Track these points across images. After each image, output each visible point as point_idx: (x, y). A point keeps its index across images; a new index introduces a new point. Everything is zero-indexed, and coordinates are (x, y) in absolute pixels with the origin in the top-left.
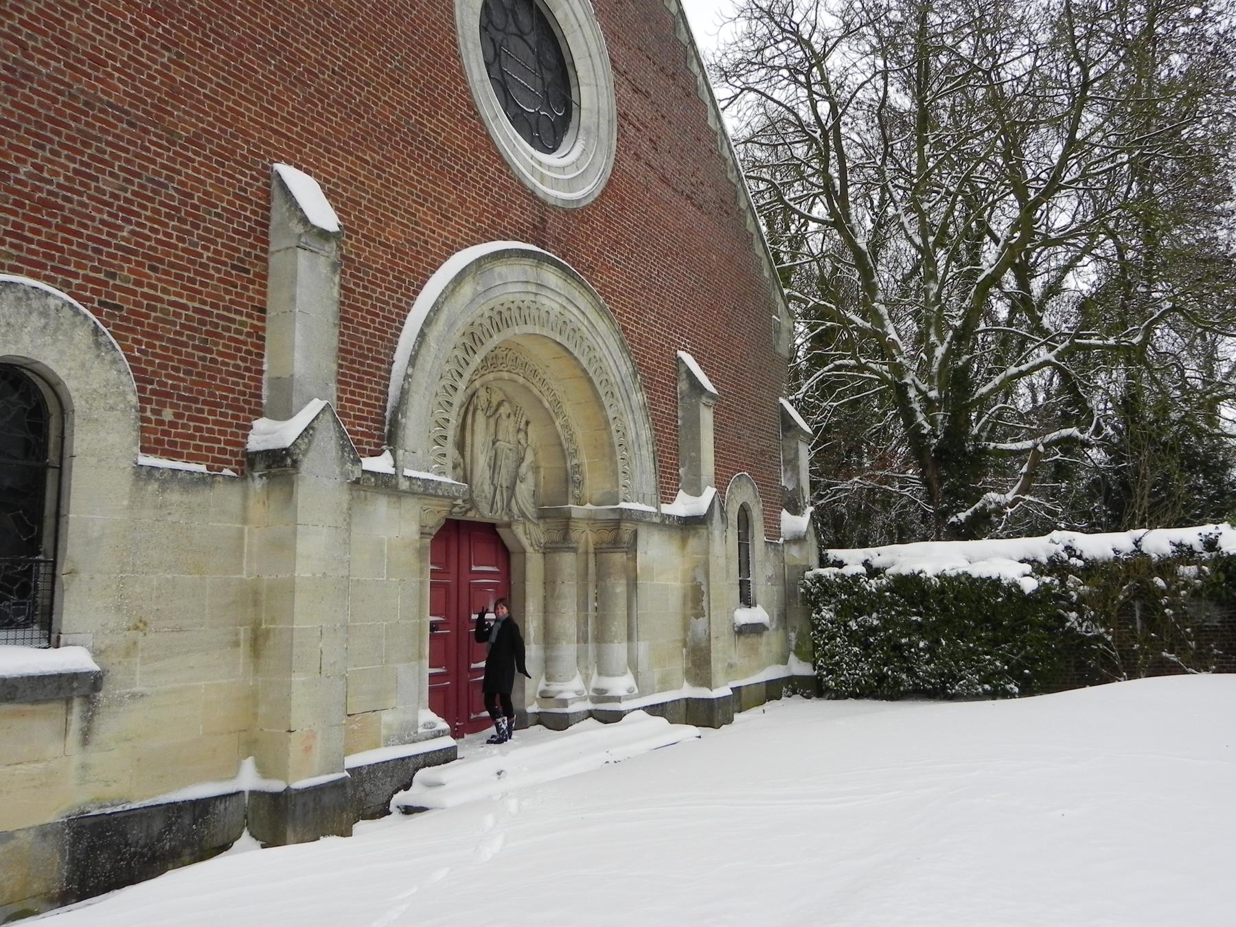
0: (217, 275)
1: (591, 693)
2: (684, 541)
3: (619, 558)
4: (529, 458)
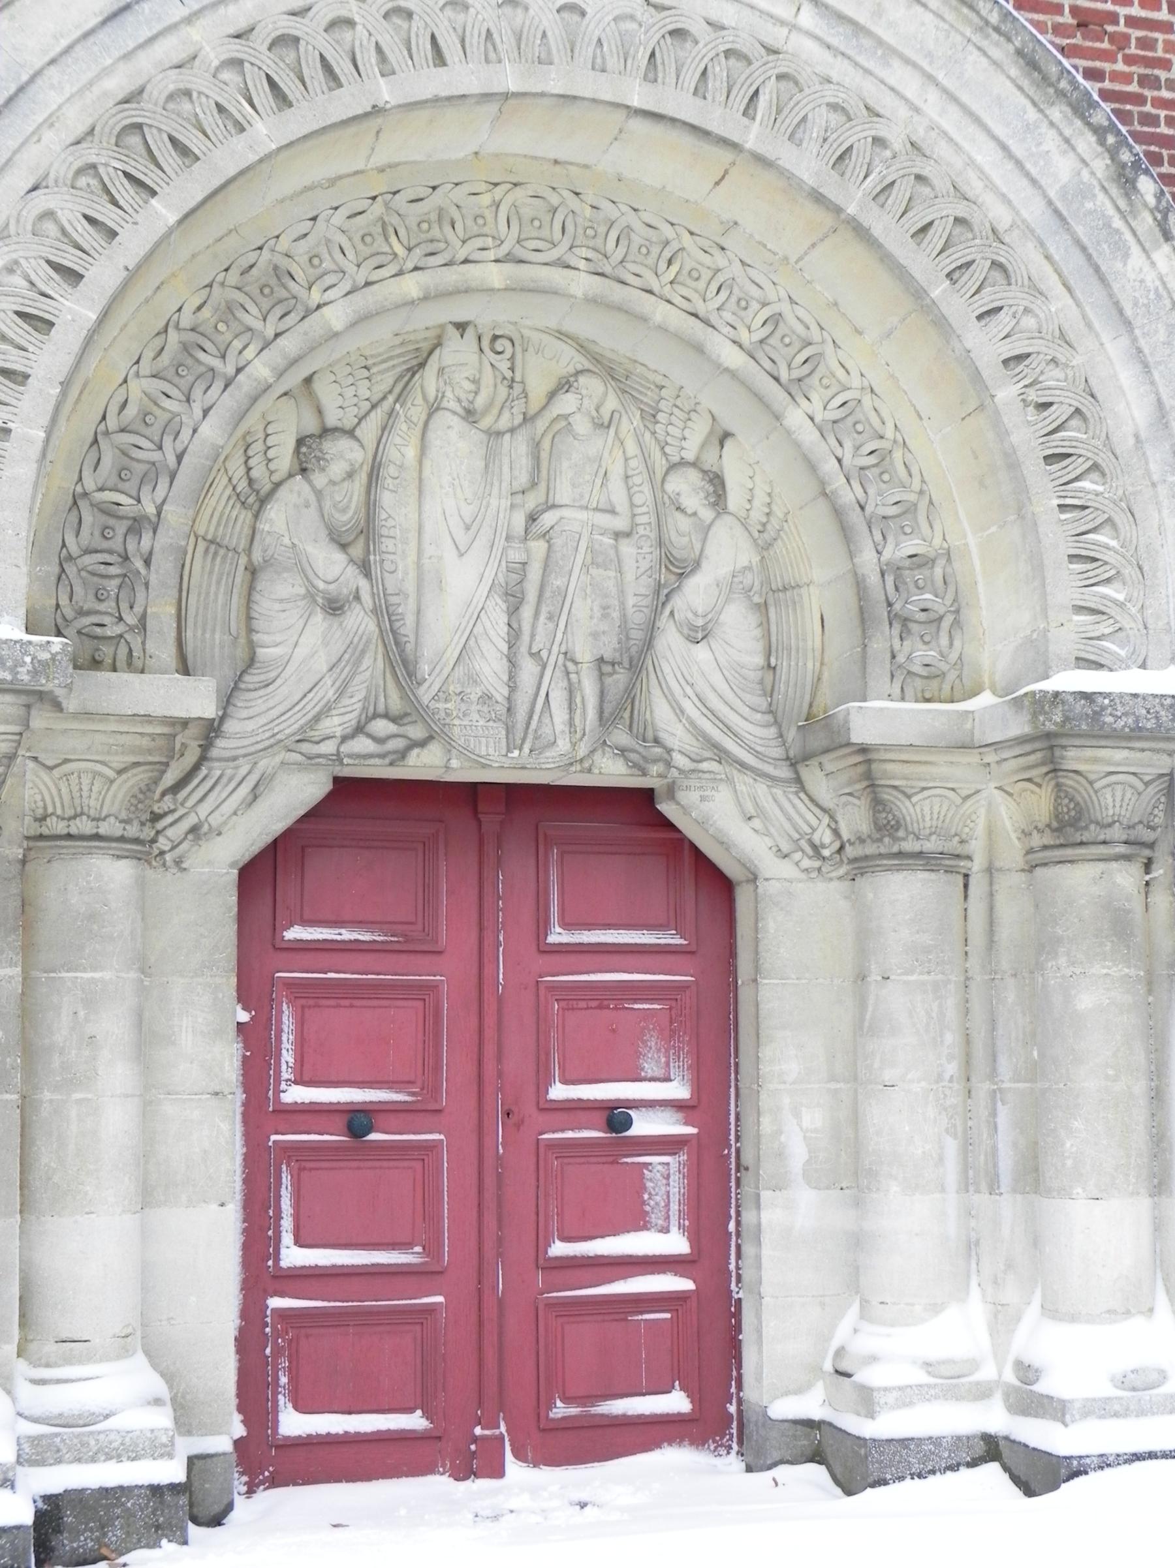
1: (1010, 1377)
4: (726, 553)
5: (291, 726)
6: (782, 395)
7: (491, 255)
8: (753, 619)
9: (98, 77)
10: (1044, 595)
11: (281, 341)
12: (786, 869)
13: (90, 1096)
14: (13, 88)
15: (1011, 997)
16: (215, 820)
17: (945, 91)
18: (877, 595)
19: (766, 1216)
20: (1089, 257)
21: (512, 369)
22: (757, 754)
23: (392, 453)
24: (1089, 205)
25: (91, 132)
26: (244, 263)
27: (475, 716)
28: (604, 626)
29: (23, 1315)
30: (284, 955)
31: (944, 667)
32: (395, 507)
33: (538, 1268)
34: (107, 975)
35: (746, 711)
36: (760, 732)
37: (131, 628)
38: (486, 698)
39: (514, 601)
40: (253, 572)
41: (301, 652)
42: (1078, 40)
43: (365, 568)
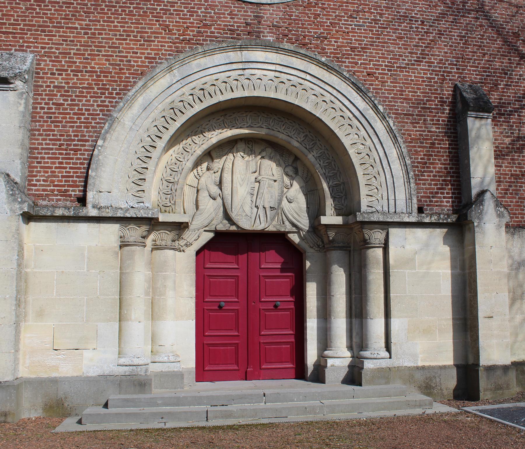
6: (307, 151)
7: (245, 126)
11: (203, 146)
12: (312, 250)
21: (220, 185)
27: (244, 219)
28: (271, 200)
31: (343, 207)
34: (168, 273)
42: (368, 78)
43: (221, 189)
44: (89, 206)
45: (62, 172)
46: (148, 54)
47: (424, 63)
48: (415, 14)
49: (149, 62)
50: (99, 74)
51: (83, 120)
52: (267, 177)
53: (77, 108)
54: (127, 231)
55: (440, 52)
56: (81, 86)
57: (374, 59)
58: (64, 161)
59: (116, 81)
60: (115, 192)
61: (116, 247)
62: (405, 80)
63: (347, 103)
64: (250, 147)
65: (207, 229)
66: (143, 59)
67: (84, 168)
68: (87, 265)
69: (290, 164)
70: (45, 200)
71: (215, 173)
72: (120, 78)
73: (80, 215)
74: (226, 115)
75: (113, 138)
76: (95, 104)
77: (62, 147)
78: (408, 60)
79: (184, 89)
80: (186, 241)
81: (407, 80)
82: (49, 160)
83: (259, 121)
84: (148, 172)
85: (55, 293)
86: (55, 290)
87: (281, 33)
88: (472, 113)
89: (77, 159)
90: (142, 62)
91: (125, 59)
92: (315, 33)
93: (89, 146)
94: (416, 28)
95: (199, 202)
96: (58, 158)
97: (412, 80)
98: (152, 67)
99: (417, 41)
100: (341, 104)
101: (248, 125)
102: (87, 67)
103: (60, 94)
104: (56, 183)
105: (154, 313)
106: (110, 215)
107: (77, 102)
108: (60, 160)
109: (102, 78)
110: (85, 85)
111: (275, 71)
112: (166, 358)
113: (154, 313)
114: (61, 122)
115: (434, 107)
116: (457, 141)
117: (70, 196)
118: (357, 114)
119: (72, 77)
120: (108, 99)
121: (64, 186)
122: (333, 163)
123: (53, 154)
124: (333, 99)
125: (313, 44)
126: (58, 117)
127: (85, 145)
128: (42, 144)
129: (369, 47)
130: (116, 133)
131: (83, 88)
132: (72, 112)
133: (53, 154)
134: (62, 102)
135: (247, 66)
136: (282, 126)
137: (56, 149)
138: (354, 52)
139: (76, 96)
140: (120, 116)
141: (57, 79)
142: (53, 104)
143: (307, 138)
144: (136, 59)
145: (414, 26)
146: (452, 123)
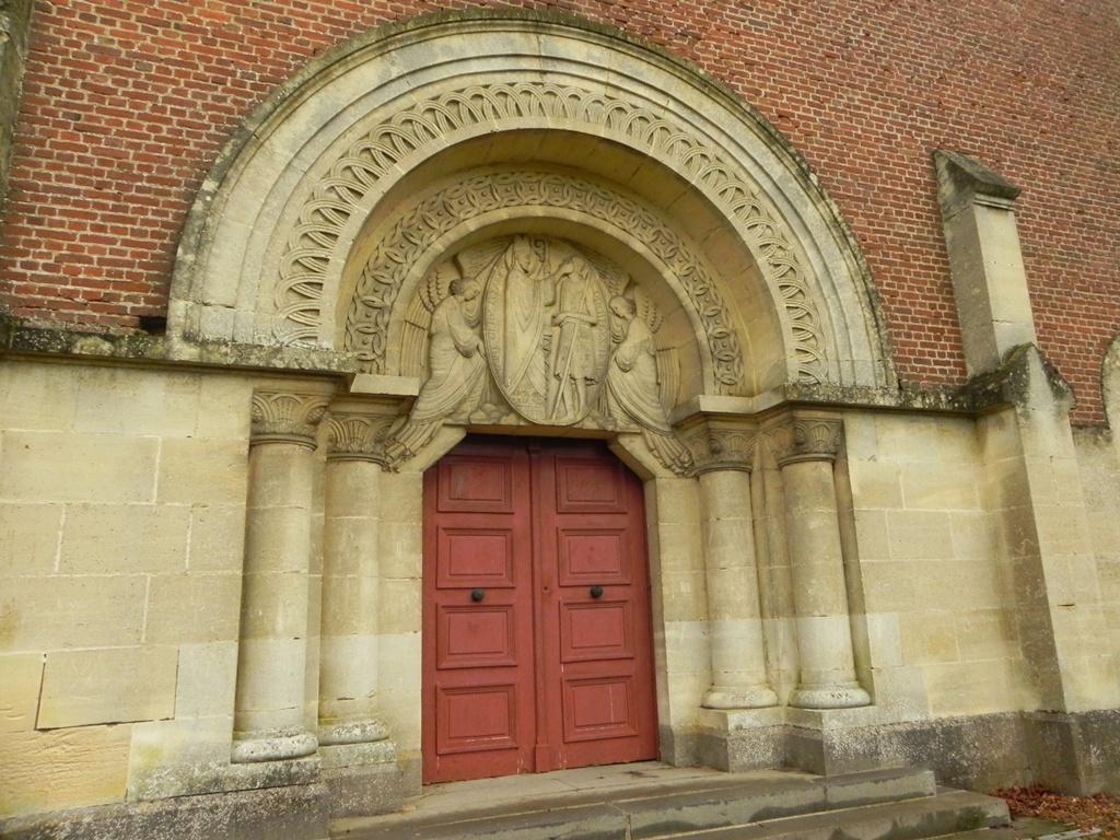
0: (1054, 301)
2: (979, 442)
3: (815, 473)
5: (448, 407)
7: (538, 202)
8: (651, 361)
9: (371, 112)
10: (783, 345)
12: (668, 473)
13: (356, 576)
14: (334, 114)
15: (775, 526)
16: (413, 448)
17: (729, 137)
18: (707, 348)
19: (668, 634)
20: (792, 206)
22: (655, 421)
23: (492, 287)
24: (790, 185)
25: (368, 135)
26: (431, 200)
29: (321, 687)
30: (443, 515)
32: (494, 311)
33: (437, 754)
34: (365, 518)
35: (649, 401)
36: (656, 411)
37: (379, 356)
38: (536, 393)
39: (547, 351)
40: (430, 337)
41: (453, 373)
43: (482, 337)
44: (175, 335)
45: (102, 251)
46: (331, 12)
47: (875, 108)
48: (853, 17)
49: (332, 30)
50: (210, 36)
51: (164, 134)
52: (576, 316)
53: (150, 104)
54: (273, 406)
55: (902, 91)
56: (163, 57)
57: (789, 89)
58: (109, 224)
59: (254, 59)
60: (246, 308)
61: (243, 442)
62: (847, 133)
63: (747, 163)
64: (541, 252)
65: (449, 421)
66: (319, 20)
67: (163, 246)
68: (159, 488)
69: (620, 292)
70: (46, 316)
71: (466, 300)
72: (264, 54)
73: (147, 354)
74: (496, 175)
75: (245, 181)
76: (199, 102)
77: (106, 191)
78: (848, 99)
79: (414, 98)
80: (403, 448)
81: (850, 134)
82: (65, 219)
83: (565, 195)
84: (329, 267)
85: (57, 563)
86: (58, 557)
87: (615, 16)
88: (982, 197)
89: (146, 222)
90: (317, 27)
91: (276, 15)
92: (679, 25)
93: (178, 195)
94: (857, 42)
95: (434, 360)
96: (94, 217)
97: (858, 136)
98: (339, 41)
99: (860, 65)
100: (736, 166)
101: (543, 200)
102: (180, 17)
103: (104, 66)
104: (81, 276)
105: (326, 619)
106: (230, 361)
107: (150, 91)
108: (98, 221)
109: (218, 47)
110: (175, 57)
111: (608, 84)
112: (357, 732)
113: (326, 619)
114: (105, 131)
115: (900, 189)
116: (946, 256)
117: (122, 311)
118: (768, 186)
119: (139, 32)
120: (232, 96)
121: (104, 285)
122: (712, 290)
123: (76, 204)
124: (720, 153)
125: (675, 44)
126: (98, 120)
127: (168, 194)
128: (48, 177)
129: (777, 64)
130: (252, 170)
131: (168, 61)
132: (136, 112)
133: (76, 204)
134: (109, 84)
135: (549, 66)
136: (610, 209)
137: (87, 194)
138: (752, 70)
139: (149, 77)
140: (263, 132)
141: (100, 31)
142: (84, 86)
143: (661, 237)
144: (303, 20)
145: (852, 38)
146: (934, 222)
